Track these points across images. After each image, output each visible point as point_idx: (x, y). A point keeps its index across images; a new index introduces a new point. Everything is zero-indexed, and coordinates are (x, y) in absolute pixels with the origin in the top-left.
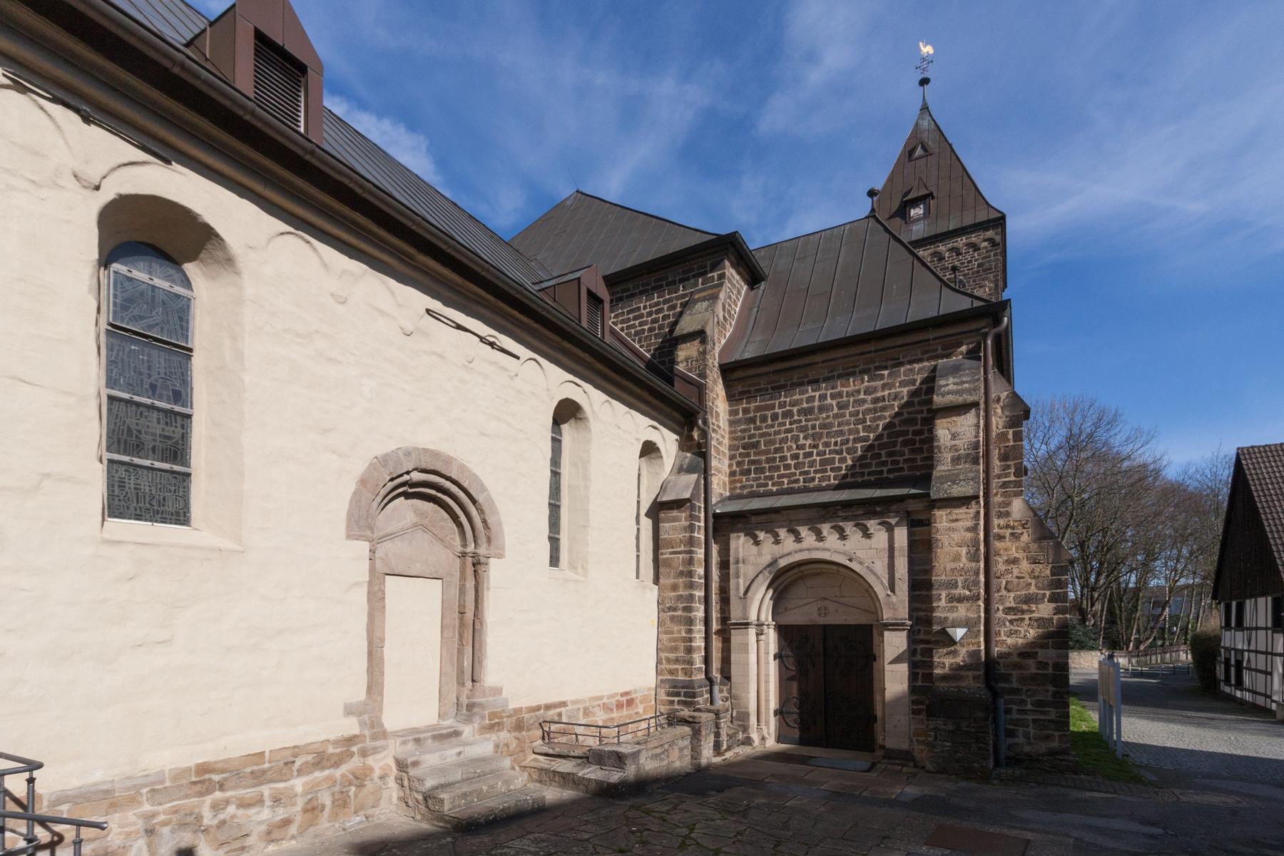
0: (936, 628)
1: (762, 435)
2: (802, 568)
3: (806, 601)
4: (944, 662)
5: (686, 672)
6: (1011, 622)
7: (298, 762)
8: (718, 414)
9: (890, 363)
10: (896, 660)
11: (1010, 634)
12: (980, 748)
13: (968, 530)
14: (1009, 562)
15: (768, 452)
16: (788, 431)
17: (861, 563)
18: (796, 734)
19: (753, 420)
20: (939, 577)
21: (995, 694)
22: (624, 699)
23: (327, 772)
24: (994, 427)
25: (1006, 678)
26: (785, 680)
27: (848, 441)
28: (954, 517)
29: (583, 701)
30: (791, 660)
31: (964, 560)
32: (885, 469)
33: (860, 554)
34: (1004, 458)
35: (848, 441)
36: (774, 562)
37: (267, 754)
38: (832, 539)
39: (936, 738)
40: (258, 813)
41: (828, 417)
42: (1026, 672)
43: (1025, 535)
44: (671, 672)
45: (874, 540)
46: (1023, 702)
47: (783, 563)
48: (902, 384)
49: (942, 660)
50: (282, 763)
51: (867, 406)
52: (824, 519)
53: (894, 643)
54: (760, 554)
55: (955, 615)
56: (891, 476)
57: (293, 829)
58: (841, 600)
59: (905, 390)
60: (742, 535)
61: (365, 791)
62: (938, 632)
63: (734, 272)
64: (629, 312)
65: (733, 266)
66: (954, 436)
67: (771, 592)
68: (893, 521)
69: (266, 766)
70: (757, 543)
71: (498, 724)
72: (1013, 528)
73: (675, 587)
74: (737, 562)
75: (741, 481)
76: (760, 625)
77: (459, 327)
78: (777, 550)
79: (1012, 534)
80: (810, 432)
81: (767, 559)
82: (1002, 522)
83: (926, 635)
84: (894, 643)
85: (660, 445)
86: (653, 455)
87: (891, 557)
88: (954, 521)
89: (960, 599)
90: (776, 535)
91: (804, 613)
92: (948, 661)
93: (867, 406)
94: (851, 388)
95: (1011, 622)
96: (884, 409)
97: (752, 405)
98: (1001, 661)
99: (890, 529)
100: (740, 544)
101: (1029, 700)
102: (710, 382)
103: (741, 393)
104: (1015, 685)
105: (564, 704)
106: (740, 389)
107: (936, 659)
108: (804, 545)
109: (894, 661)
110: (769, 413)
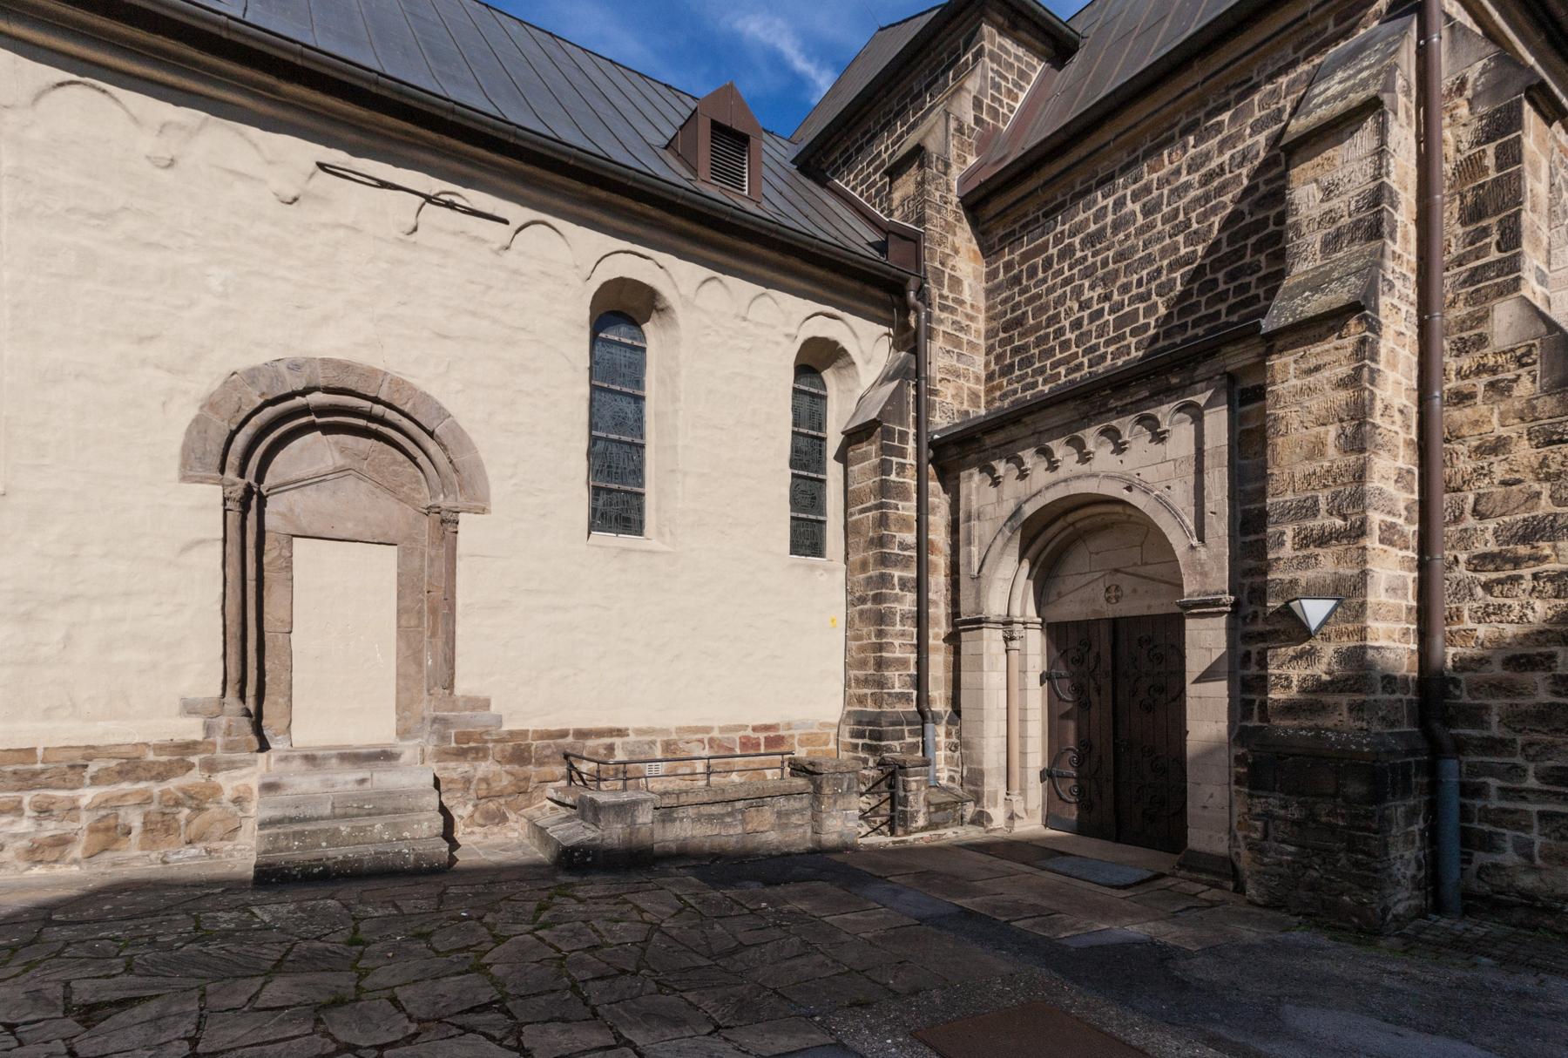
0: (1274, 604)
1: (1029, 301)
2: (1071, 518)
3: (1089, 577)
4: (1290, 675)
5: (878, 700)
6: (1488, 587)
7: (93, 768)
8: (956, 283)
9: (1233, 94)
10: (1207, 676)
11: (1485, 615)
12: (1357, 864)
13: (1342, 384)
14: (1483, 450)
15: (1037, 327)
16: (1067, 282)
17: (1147, 492)
18: (1072, 813)
19: (1017, 280)
20: (1281, 495)
21: (1436, 751)
22: (762, 736)
23: (142, 785)
24: (1449, 150)
25: (1476, 716)
26: (1055, 720)
27: (1159, 271)
28: (1313, 362)
29: (666, 731)
30: (1067, 683)
31: (1331, 451)
32: (1223, 307)
33: (1149, 475)
34: (1473, 214)
35: (1159, 271)
36: (1018, 511)
37: (40, 752)
38: (1103, 456)
39: (1266, 836)
40: (13, 823)
41: (1127, 237)
42: (1525, 702)
43: (1526, 381)
44: (861, 700)
45: (1169, 444)
46: (1517, 771)
47: (1029, 510)
48: (1257, 128)
49: (1285, 671)
50: (64, 766)
51: (1192, 194)
52: (1086, 420)
53: (1206, 641)
54: (1000, 500)
55: (1310, 574)
56: (1235, 318)
57: (77, 852)
58: (1143, 570)
59: (1262, 138)
60: (975, 471)
61: (205, 816)
62: (1278, 612)
63: (1008, 44)
64: (869, 165)
65: (1002, 31)
66: (1328, 192)
67: (1026, 565)
68: (1201, 399)
69: (39, 766)
70: (996, 482)
71: (477, 750)
72: (1494, 371)
73: (864, 566)
74: (969, 519)
75: (1000, 387)
76: (1008, 623)
77: (384, 185)
78: (1023, 488)
79: (1492, 385)
80: (1100, 273)
81: (1009, 507)
82: (1466, 362)
83: (1260, 621)
84: (1206, 641)
85: (847, 342)
86: (841, 363)
87: (1200, 472)
88: (1309, 372)
89: (1323, 540)
90: (1020, 463)
91: (1084, 598)
92: (1297, 673)
93: (1192, 194)
94: (1168, 168)
95: (1488, 587)
96: (1221, 190)
97: (1016, 256)
98: (1461, 677)
99: (1197, 415)
100: (973, 484)
101: (1531, 768)
102: (934, 228)
103: (1002, 239)
104: (1496, 731)
105: (620, 733)
106: (1001, 232)
107: (1273, 670)
108: (1062, 473)
109: (1203, 678)
110: (1039, 260)
